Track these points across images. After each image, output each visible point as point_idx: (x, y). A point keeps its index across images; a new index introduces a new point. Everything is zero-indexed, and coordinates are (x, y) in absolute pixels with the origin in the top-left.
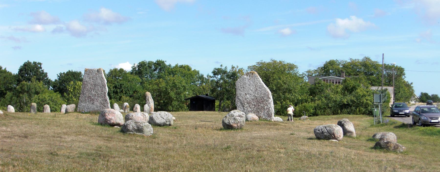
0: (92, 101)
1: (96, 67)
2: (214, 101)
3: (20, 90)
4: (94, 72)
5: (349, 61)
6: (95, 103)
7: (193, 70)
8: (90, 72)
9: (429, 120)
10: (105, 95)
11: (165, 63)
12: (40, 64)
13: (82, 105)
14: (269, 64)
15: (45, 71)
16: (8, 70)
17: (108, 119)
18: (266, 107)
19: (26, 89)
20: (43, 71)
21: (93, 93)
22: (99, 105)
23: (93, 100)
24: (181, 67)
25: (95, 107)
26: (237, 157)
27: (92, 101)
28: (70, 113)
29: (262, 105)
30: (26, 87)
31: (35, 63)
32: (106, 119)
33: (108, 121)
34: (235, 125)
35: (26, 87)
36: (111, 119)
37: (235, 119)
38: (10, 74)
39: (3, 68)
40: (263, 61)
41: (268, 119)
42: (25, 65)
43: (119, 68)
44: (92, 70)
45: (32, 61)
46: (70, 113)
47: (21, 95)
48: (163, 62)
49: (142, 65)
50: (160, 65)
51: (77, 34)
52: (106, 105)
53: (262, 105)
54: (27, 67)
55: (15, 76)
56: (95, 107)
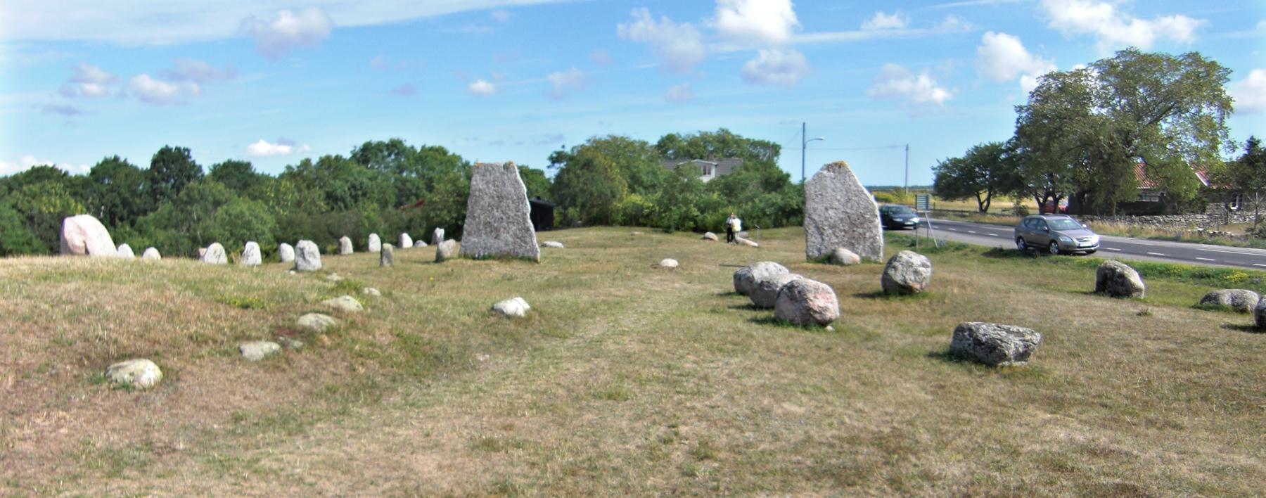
0: (495, 231)
1: (502, 161)
5: (698, 135)
6: (503, 235)
8: (487, 170)
9: (1077, 242)
10: (525, 220)
12: (188, 150)
14: (606, 142)
15: (198, 163)
16: (130, 162)
17: (816, 309)
18: (868, 235)
21: (497, 214)
22: (510, 239)
23: (497, 230)
24: (431, 149)
25: (502, 244)
26: (1120, 388)
27: (495, 231)
29: (861, 231)
31: (178, 149)
32: (809, 309)
33: (817, 316)
34: (917, 286)
36: (826, 309)
37: (916, 272)
38: (135, 169)
39: (122, 160)
41: (873, 258)
43: (334, 155)
44: (491, 166)
45: (173, 146)
46: (448, 259)
48: (401, 142)
49: (367, 148)
50: (395, 147)
51: (146, 98)
52: (528, 240)
53: (861, 231)
55: (146, 173)
56: (502, 244)
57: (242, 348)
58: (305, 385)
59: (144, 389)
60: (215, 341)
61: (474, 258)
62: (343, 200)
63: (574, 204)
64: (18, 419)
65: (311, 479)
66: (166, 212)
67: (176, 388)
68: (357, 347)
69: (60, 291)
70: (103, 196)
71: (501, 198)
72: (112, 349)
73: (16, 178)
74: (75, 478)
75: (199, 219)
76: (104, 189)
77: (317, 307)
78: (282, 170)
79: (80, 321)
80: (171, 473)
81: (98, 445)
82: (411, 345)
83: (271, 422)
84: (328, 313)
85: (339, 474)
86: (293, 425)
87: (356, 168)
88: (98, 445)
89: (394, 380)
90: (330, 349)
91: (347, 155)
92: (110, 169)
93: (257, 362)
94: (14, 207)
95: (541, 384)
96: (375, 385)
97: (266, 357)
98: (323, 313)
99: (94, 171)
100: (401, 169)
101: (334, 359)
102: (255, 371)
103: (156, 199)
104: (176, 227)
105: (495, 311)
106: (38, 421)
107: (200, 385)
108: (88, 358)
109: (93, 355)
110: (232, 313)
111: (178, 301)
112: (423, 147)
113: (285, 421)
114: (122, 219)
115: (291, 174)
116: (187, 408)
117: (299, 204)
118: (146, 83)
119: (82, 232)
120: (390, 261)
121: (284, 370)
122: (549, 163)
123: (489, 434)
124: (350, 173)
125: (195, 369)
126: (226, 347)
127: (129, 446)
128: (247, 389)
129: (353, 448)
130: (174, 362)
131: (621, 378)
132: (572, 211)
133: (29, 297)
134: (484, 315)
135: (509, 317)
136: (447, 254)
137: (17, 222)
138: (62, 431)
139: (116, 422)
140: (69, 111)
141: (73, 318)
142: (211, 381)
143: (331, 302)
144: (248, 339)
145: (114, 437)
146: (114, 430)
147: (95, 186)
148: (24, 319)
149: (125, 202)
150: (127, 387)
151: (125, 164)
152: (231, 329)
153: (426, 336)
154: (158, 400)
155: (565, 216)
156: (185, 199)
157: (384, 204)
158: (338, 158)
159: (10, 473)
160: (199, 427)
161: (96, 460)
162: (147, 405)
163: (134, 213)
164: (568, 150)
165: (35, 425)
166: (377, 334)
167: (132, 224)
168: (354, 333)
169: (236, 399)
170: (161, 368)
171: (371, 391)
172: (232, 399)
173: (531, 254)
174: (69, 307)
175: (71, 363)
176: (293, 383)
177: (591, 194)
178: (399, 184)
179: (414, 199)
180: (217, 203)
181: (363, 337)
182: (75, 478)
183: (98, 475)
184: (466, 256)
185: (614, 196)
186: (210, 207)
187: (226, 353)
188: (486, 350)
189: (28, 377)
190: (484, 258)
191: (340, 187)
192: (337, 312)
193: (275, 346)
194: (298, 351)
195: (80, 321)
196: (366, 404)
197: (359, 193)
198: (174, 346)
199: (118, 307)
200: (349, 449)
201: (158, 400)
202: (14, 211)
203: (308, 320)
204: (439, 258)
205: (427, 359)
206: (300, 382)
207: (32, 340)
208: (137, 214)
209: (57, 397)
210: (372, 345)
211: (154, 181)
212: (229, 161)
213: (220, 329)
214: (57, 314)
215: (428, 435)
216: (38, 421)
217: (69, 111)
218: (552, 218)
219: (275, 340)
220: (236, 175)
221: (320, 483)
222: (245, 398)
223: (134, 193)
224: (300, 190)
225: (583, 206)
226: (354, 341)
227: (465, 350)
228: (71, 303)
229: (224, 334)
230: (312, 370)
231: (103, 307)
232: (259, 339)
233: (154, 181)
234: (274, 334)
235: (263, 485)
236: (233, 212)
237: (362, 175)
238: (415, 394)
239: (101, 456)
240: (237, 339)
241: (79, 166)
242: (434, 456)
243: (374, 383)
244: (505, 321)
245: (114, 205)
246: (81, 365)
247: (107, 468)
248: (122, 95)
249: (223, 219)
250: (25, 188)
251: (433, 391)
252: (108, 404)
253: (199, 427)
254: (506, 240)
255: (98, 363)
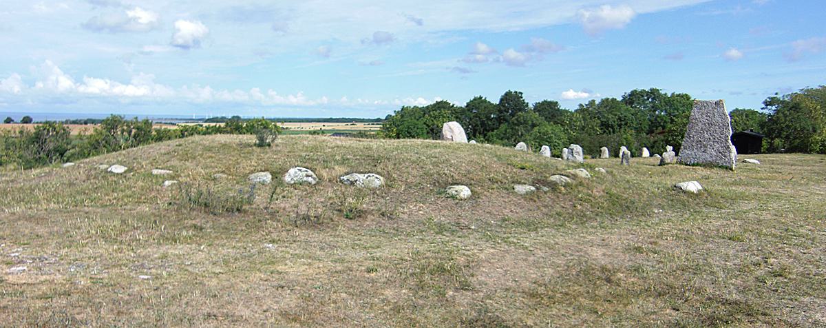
0: (704, 148)
2: (760, 139)
3: (516, 122)
4: (709, 104)
7: (692, 99)
10: (726, 140)
11: (660, 92)
12: (521, 93)
13: (684, 152)
19: (522, 121)
20: (524, 100)
27: (704, 148)
28: (668, 164)
30: (522, 118)
35: (522, 118)
40: (809, 88)
42: (506, 94)
43: (611, 98)
46: (668, 164)
47: (517, 127)
49: (633, 94)
50: (653, 93)
51: (510, 63)
54: (508, 97)
55: (496, 105)
57: (515, 187)
58: (544, 210)
59: (461, 200)
60: (502, 183)
61: (686, 165)
62: (612, 127)
63: (779, 136)
64: (402, 204)
65: (532, 249)
66: (503, 129)
67: (477, 201)
68: (580, 196)
69: (431, 152)
70: (471, 119)
71: (711, 125)
72: (450, 180)
73: (428, 107)
74: (422, 232)
75: (522, 135)
76: (472, 116)
77: (563, 173)
78: (577, 107)
79: (438, 166)
80: (465, 237)
81: (435, 220)
82: (614, 200)
83: (521, 224)
84: (568, 176)
85: (547, 249)
86: (532, 227)
87: (624, 107)
88: (435, 220)
89: (597, 215)
90: (564, 194)
91: (619, 99)
92: (478, 103)
93: (521, 195)
94: (425, 123)
95: (687, 227)
96: (585, 215)
97: (527, 193)
98: (565, 176)
99: (468, 105)
100: (655, 108)
101: (565, 199)
102: (519, 199)
103: (495, 120)
104: (508, 139)
105: (676, 188)
106: (411, 207)
107: (489, 202)
108: (438, 182)
109: (441, 181)
110: (514, 170)
111: (488, 162)
112: (673, 94)
113: (528, 225)
114: (480, 133)
115: (582, 110)
116: (480, 211)
117: (583, 128)
118: (512, 53)
119: (452, 131)
120: (627, 162)
121: (535, 201)
122: (763, 106)
123: (640, 244)
124: (619, 110)
125: (488, 194)
126: (507, 186)
127: (449, 223)
128: (513, 208)
129: (560, 240)
130: (478, 189)
131: (746, 231)
132: (777, 141)
133: (417, 153)
134: (668, 189)
135: (685, 192)
136: (668, 161)
137: (425, 131)
138: (420, 212)
139: (446, 212)
140: (465, 71)
141: (435, 164)
142: (495, 201)
143: (572, 171)
144: (519, 183)
145: (443, 219)
146: (443, 216)
147: (468, 113)
148: (413, 162)
149: (483, 123)
150: (453, 197)
151: (485, 101)
152: (511, 178)
153: (626, 196)
154: (467, 205)
155: (771, 144)
156: (516, 122)
157: (638, 130)
158: (614, 100)
159: (395, 225)
160: (484, 220)
161: (432, 226)
162: (461, 207)
163: (486, 130)
164: (780, 96)
165: (410, 208)
166: (594, 191)
167: (485, 136)
168: (580, 188)
169: (506, 211)
170: (471, 191)
171: (582, 219)
172: (504, 211)
173: (728, 165)
174: (434, 159)
175: (430, 184)
176: (538, 208)
177: (795, 129)
178: (653, 119)
179: (660, 128)
180: (534, 126)
181: (585, 191)
182: (422, 232)
183: (432, 232)
184: (681, 163)
185: (815, 131)
186: (529, 128)
187: (506, 189)
188: (661, 207)
189: (410, 187)
190: (693, 165)
191: (612, 118)
192: (575, 176)
193: (533, 188)
194: (545, 193)
195: (438, 166)
196: (576, 223)
197: (623, 123)
198: (481, 183)
199: (457, 161)
200: (556, 240)
201: (467, 205)
202: (425, 125)
203: (553, 178)
204: (662, 163)
205: (621, 207)
206: (542, 208)
207: (415, 172)
208: (488, 131)
209: (421, 198)
210: (590, 195)
211: (500, 111)
212: (545, 101)
213: (506, 177)
214: (428, 161)
215: (603, 240)
216: (411, 207)
217: (465, 71)
218: (761, 146)
219: (533, 186)
220: (549, 110)
221: (535, 251)
222: (511, 211)
223: (489, 118)
224: (585, 119)
225: (787, 137)
226: (579, 192)
227: (649, 205)
228: (436, 157)
229: (507, 180)
230: (550, 203)
231: (450, 161)
232: (525, 184)
233: (500, 111)
234: (533, 183)
235: (506, 247)
236: (542, 131)
237: (627, 111)
238: (607, 222)
239: (435, 225)
240: (513, 182)
241: (460, 102)
242: (602, 250)
243: (584, 214)
244: (682, 194)
245: (477, 125)
246: (435, 185)
247: (437, 230)
248: (497, 61)
249: (536, 135)
250: (431, 113)
251: (618, 223)
252: (443, 204)
253: (484, 220)
254: (711, 153)
255: (442, 186)
